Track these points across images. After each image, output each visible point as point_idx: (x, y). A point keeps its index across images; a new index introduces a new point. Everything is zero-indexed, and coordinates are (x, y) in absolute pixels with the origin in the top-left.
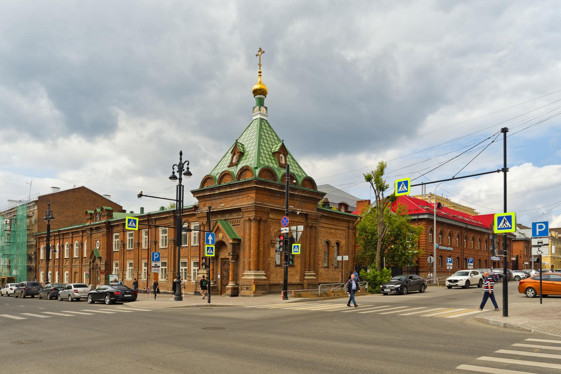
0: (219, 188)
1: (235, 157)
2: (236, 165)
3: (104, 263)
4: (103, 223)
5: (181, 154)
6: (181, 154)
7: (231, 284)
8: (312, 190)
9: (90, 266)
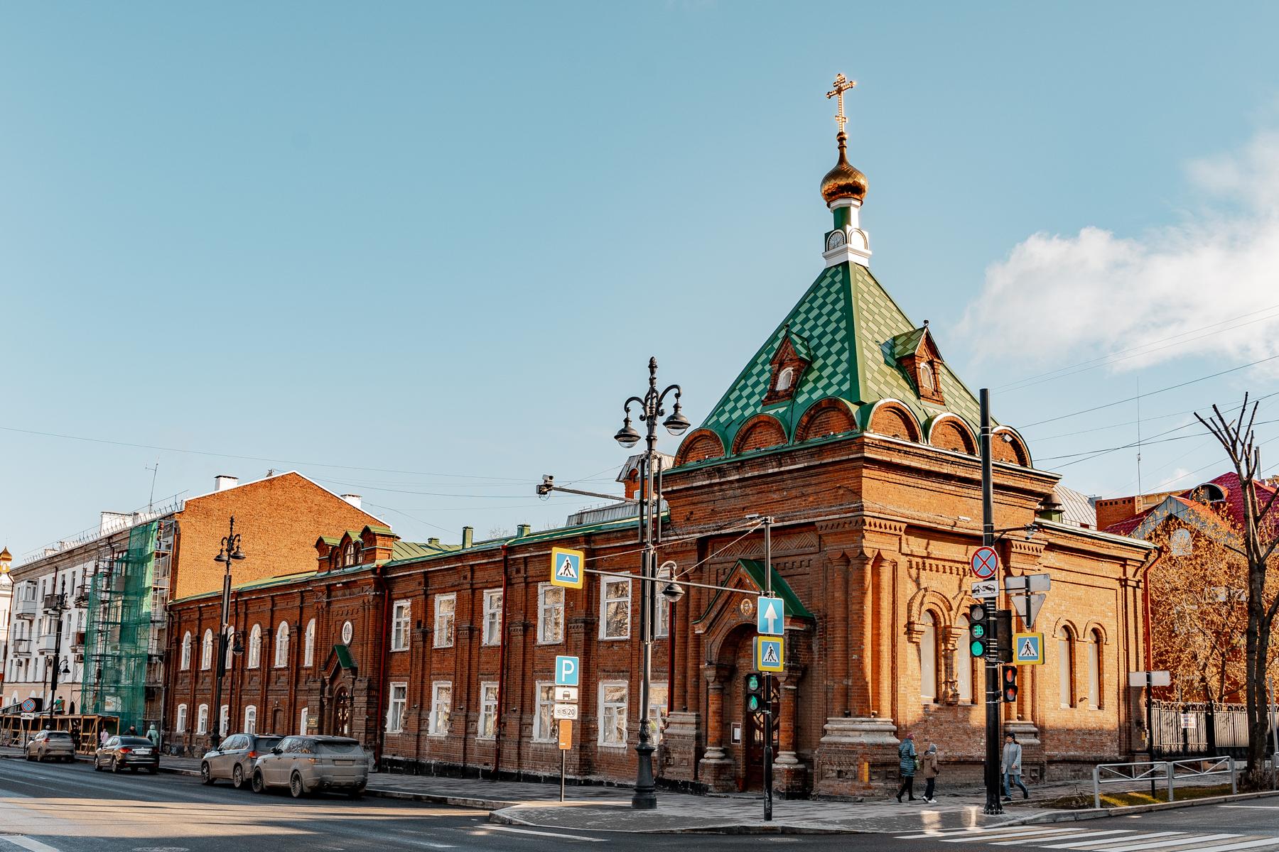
0: (741, 466)
1: (783, 375)
2: (791, 394)
3: (364, 685)
4: (366, 572)
5: (652, 367)
6: (652, 367)
7: (785, 760)
8: (1018, 467)
9: (322, 692)
